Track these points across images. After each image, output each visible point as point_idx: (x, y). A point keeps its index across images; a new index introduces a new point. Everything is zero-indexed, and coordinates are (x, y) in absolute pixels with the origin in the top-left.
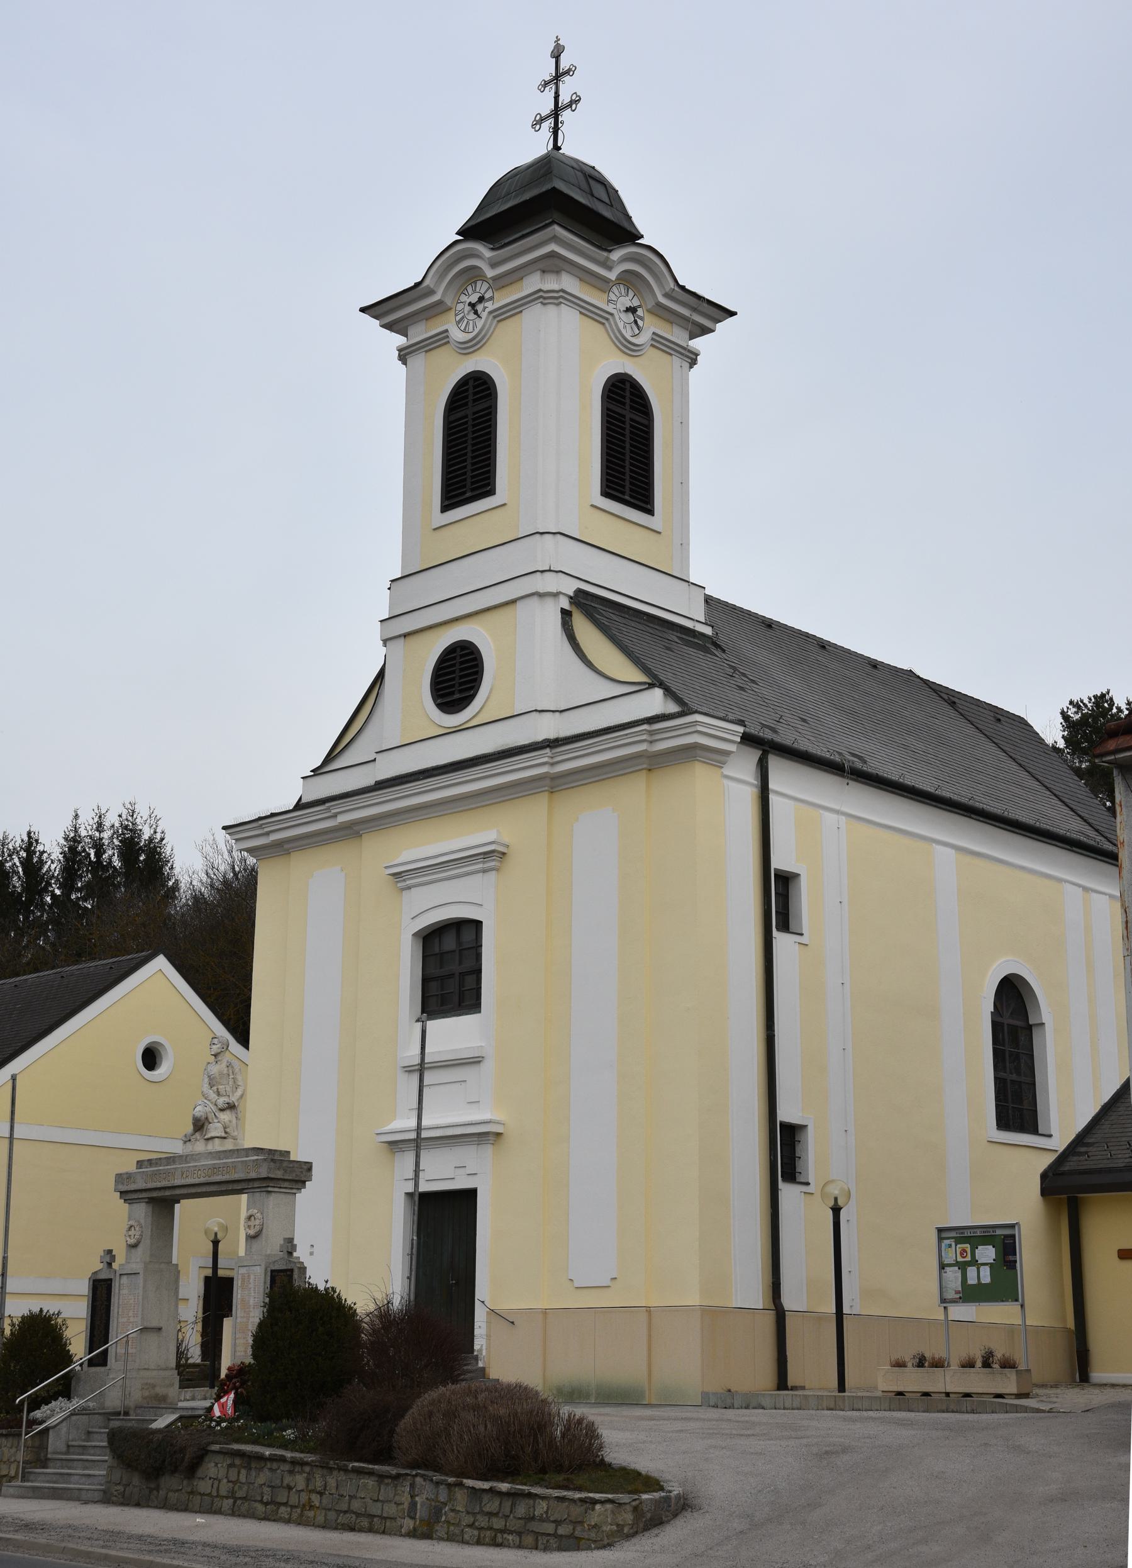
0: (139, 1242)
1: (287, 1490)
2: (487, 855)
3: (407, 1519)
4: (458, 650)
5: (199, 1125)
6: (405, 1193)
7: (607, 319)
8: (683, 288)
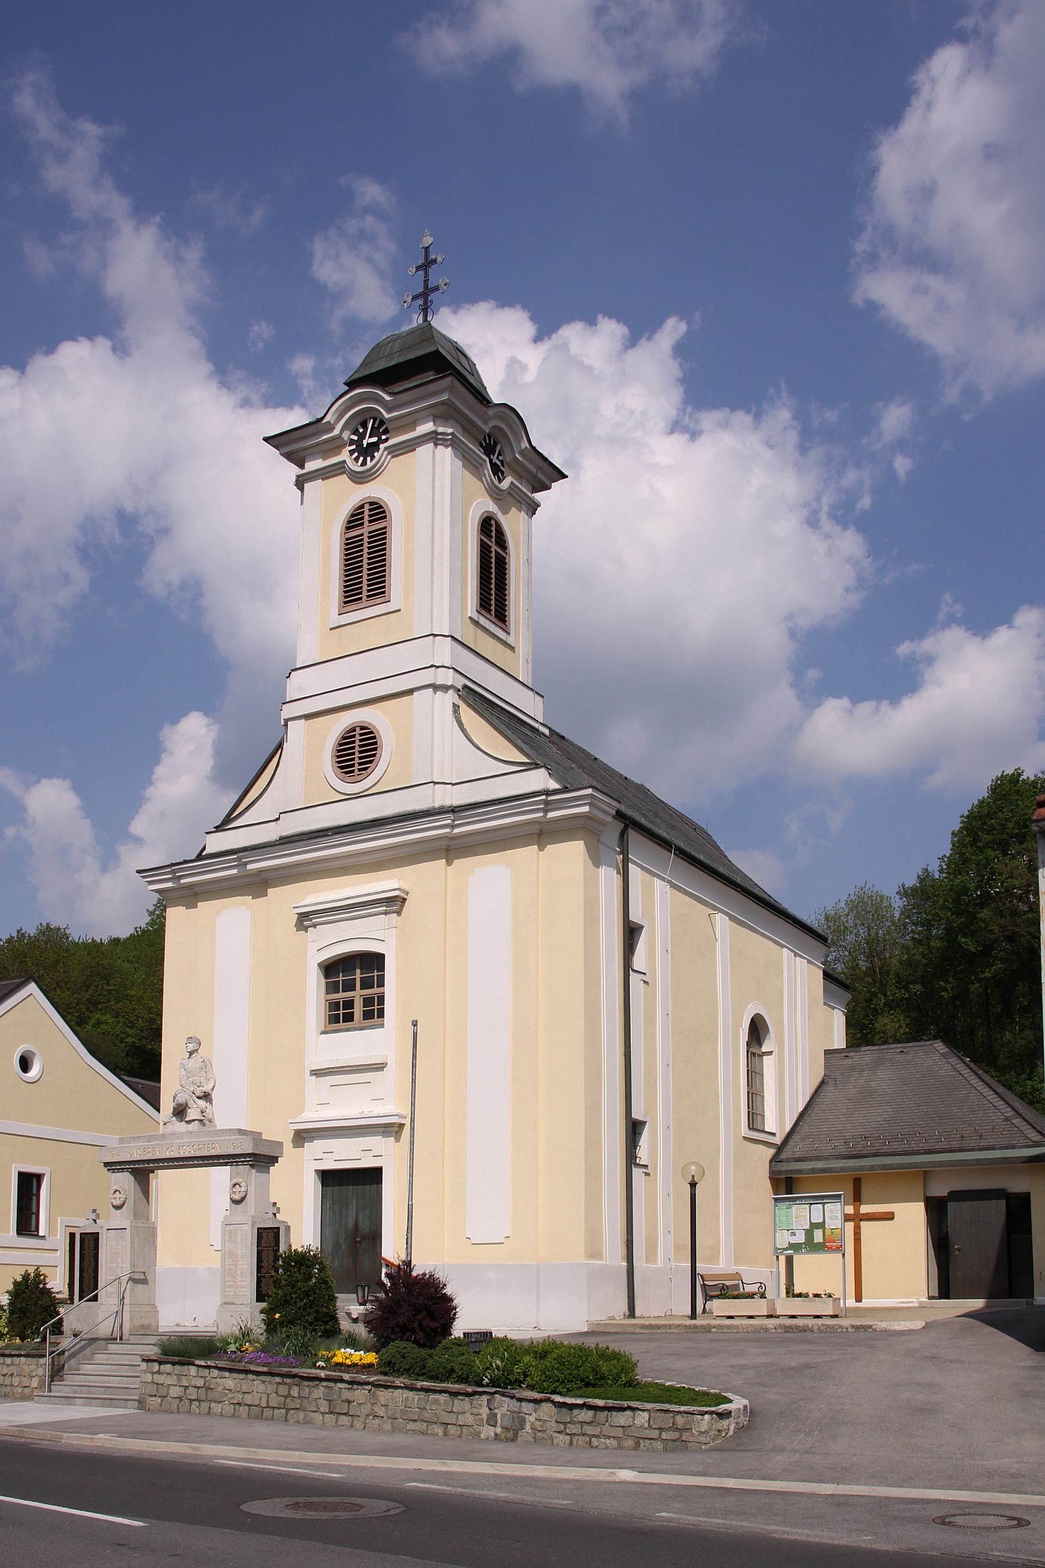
1: (346, 1403)
2: (389, 901)
3: (486, 1426)
4: (358, 729)
6: (315, 1170)
7: (481, 465)
8: (534, 448)
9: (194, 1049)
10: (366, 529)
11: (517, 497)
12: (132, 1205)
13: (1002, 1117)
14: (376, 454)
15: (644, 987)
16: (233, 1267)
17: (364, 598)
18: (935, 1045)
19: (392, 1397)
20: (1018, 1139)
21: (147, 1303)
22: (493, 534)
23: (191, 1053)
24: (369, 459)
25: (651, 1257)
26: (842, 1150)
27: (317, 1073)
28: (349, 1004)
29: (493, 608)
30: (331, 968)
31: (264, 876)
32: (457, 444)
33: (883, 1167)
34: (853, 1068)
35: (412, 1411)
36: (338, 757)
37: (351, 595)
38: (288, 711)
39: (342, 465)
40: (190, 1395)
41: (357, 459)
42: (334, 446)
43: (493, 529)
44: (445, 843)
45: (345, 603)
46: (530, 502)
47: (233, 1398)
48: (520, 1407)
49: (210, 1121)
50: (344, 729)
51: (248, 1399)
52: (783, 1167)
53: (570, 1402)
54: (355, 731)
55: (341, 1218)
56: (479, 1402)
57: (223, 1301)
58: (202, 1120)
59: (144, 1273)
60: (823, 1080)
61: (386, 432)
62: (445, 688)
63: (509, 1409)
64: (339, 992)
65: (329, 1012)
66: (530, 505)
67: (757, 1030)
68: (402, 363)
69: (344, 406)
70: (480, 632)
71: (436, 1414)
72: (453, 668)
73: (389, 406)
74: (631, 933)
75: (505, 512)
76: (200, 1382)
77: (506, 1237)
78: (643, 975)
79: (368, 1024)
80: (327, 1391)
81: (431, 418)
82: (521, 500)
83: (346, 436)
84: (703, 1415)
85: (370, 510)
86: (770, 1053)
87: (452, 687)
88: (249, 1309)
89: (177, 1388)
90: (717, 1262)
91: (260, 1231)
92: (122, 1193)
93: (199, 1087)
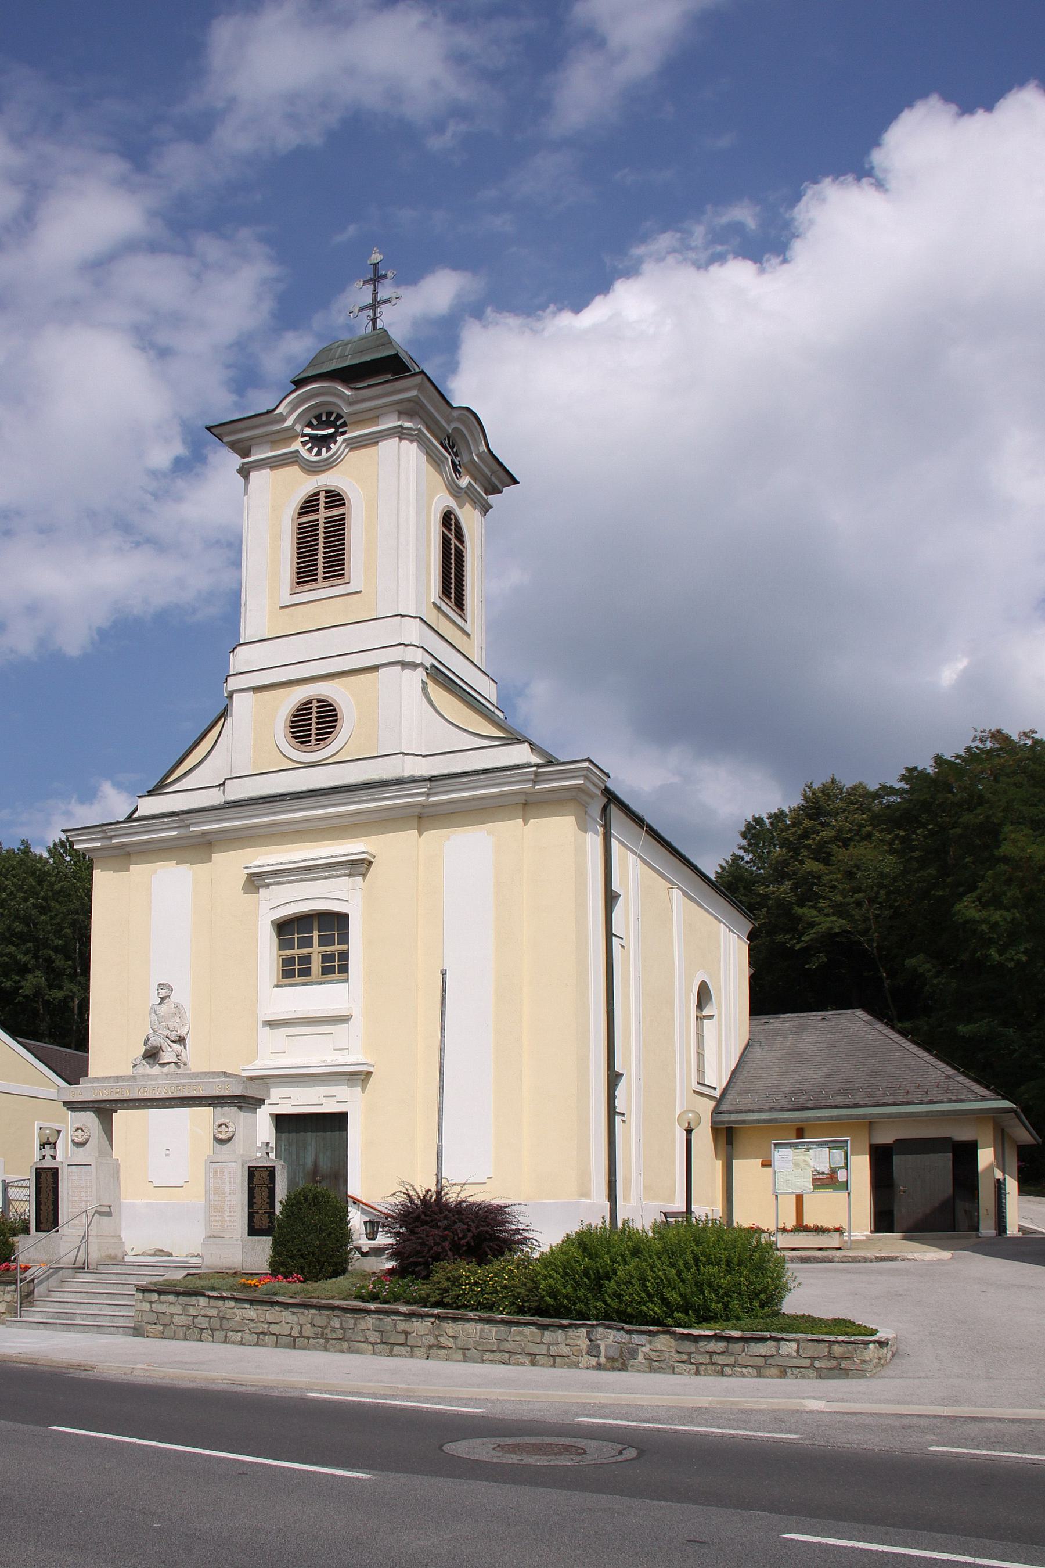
0: (87, 1142)
1: (403, 1334)
3: (586, 1356)
4: (315, 702)
5: (152, 1055)
6: (270, 1114)
7: (443, 462)
8: (491, 453)
9: (166, 995)
10: (322, 515)
11: (472, 496)
12: (97, 1142)
13: (944, 1075)
14: (332, 446)
15: (622, 951)
16: (220, 1203)
17: (320, 579)
18: (857, 1014)
19: (462, 1329)
20: (965, 1094)
21: (113, 1235)
22: (453, 527)
23: (162, 999)
24: (324, 450)
25: (626, 1198)
26: (785, 1103)
27: (271, 1024)
28: (306, 959)
29: (453, 596)
30: (284, 927)
31: (208, 837)
32: (422, 440)
33: (831, 1118)
34: (776, 1033)
35: (489, 1343)
36: (292, 727)
37: (305, 574)
38: (233, 684)
39: (295, 454)
40: (200, 1324)
41: (310, 450)
42: (289, 435)
43: (453, 522)
44: (417, 810)
45: (298, 583)
46: (484, 503)
47: (256, 1327)
48: (631, 1339)
49: (185, 1064)
50: (328, 696)
51: (275, 1329)
52: (725, 1117)
53: (697, 1334)
54: (311, 703)
55: (298, 1157)
56: (577, 1334)
57: (209, 1234)
58: (177, 1063)
59: (110, 1207)
60: (749, 1042)
61: (344, 425)
62: (414, 666)
63: (616, 1340)
64: (294, 949)
65: (282, 967)
66: (483, 506)
67: (704, 995)
68: (357, 364)
69: (296, 400)
70: (441, 617)
71: (521, 1345)
72: (423, 647)
73: (350, 400)
74: (611, 898)
75: (461, 507)
76: (213, 1312)
77: (488, 1178)
78: (620, 940)
79: (326, 979)
80: (377, 1322)
81: (397, 413)
82: (476, 500)
83: (298, 428)
84: (868, 1344)
85: (326, 498)
86: (711, 1017)
87: (421, 665)
88: (239, 1242)
89: (183, 1317)
90: (673, 1202)
91: (251, 1169)
92: (85, 1131)
93: (172, 1031)
